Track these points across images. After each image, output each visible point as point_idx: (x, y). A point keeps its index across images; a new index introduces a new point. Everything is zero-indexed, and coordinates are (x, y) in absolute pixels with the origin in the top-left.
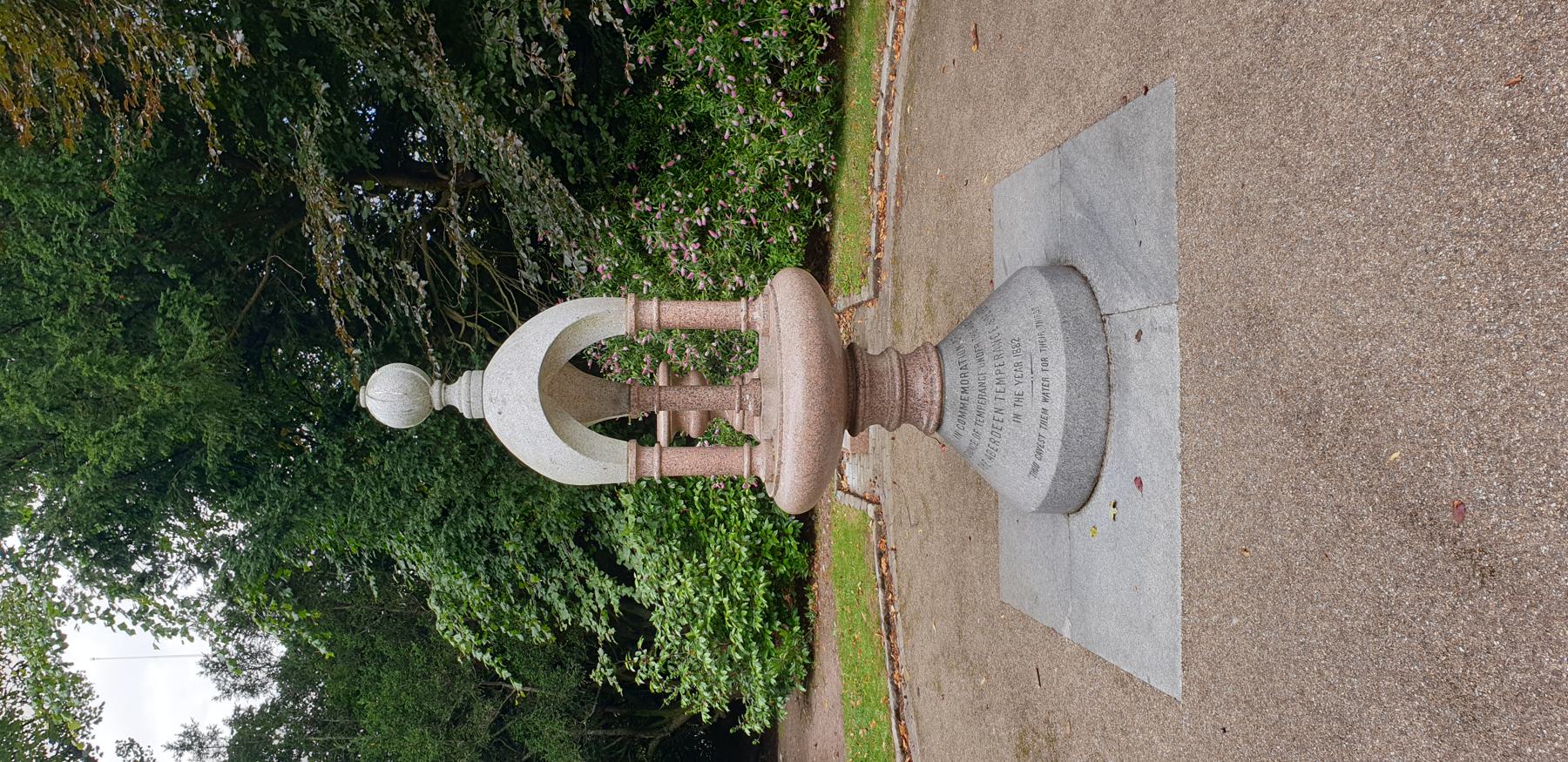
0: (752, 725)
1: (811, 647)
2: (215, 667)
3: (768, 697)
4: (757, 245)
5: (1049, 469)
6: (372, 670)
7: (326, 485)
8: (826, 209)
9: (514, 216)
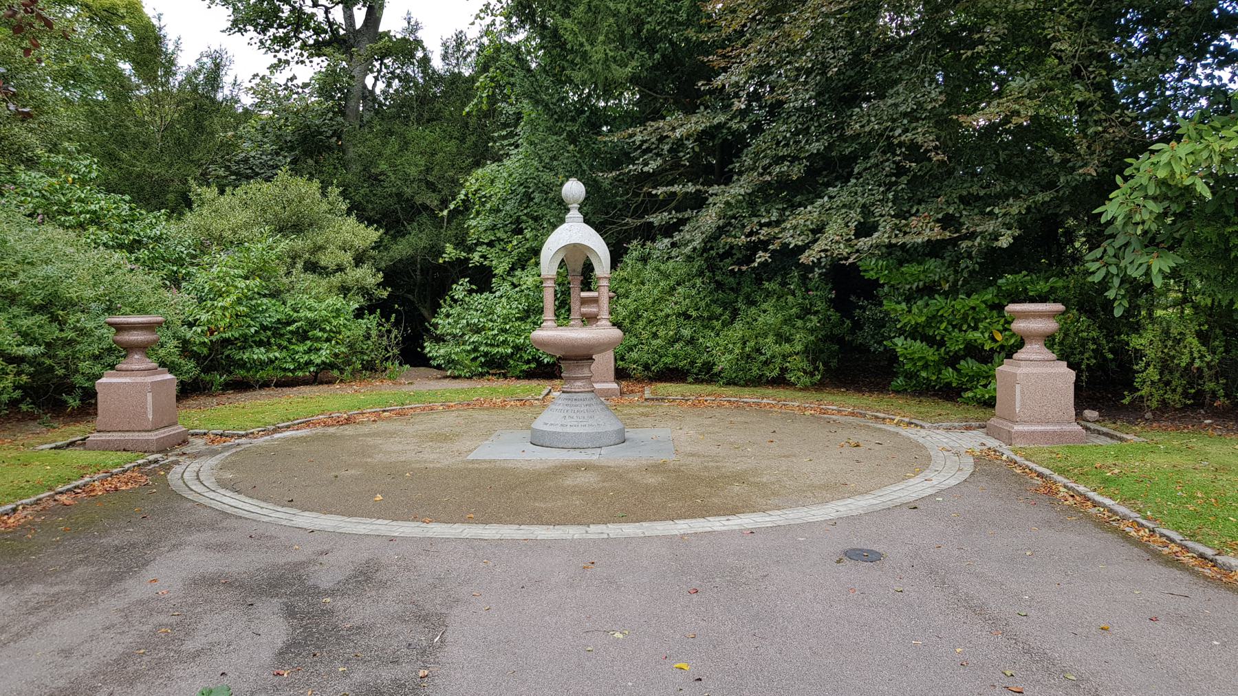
0: (430, 348)
2: (460, 42)
6: (456, 134)
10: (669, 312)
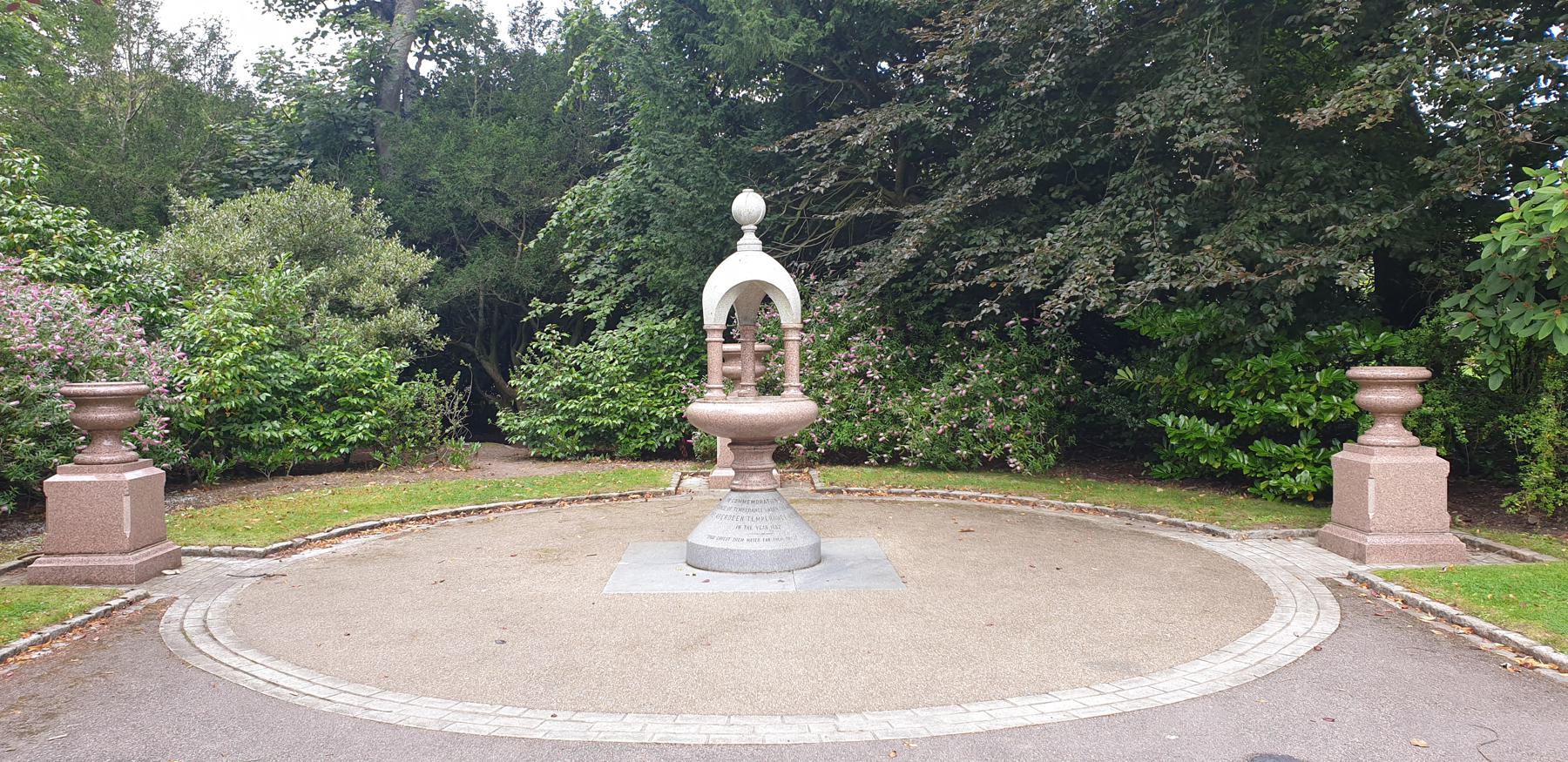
0: (503, 418)
1: (564, 459)
3: (526, 429)
4: (854, 413)
5: (711, 544)
6: (533, 129)
8: (881, 462)
9: (873, 246)
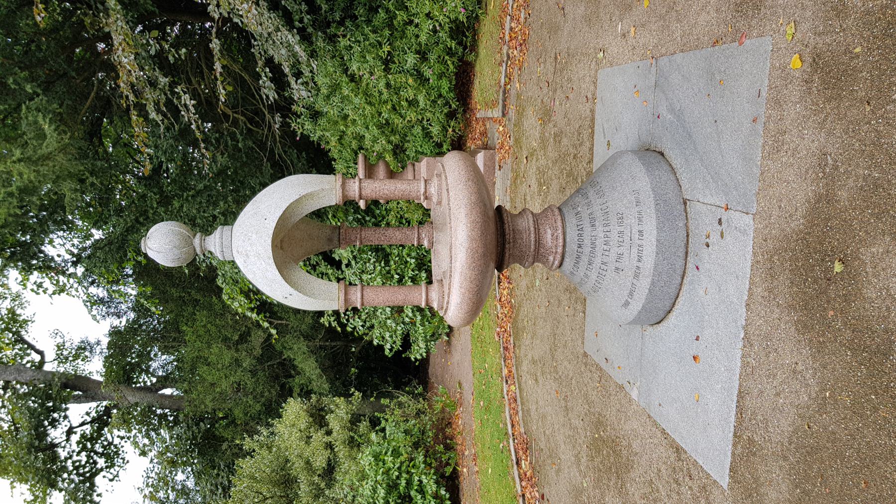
3: (426, 341)
6: (190, 309)
7: (148, 217)
10: (382, 85)
